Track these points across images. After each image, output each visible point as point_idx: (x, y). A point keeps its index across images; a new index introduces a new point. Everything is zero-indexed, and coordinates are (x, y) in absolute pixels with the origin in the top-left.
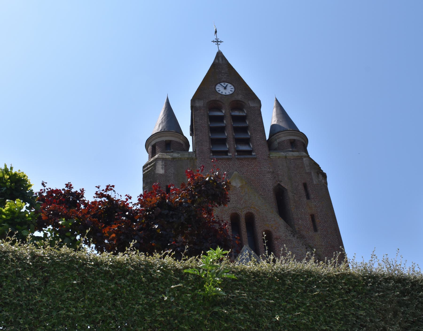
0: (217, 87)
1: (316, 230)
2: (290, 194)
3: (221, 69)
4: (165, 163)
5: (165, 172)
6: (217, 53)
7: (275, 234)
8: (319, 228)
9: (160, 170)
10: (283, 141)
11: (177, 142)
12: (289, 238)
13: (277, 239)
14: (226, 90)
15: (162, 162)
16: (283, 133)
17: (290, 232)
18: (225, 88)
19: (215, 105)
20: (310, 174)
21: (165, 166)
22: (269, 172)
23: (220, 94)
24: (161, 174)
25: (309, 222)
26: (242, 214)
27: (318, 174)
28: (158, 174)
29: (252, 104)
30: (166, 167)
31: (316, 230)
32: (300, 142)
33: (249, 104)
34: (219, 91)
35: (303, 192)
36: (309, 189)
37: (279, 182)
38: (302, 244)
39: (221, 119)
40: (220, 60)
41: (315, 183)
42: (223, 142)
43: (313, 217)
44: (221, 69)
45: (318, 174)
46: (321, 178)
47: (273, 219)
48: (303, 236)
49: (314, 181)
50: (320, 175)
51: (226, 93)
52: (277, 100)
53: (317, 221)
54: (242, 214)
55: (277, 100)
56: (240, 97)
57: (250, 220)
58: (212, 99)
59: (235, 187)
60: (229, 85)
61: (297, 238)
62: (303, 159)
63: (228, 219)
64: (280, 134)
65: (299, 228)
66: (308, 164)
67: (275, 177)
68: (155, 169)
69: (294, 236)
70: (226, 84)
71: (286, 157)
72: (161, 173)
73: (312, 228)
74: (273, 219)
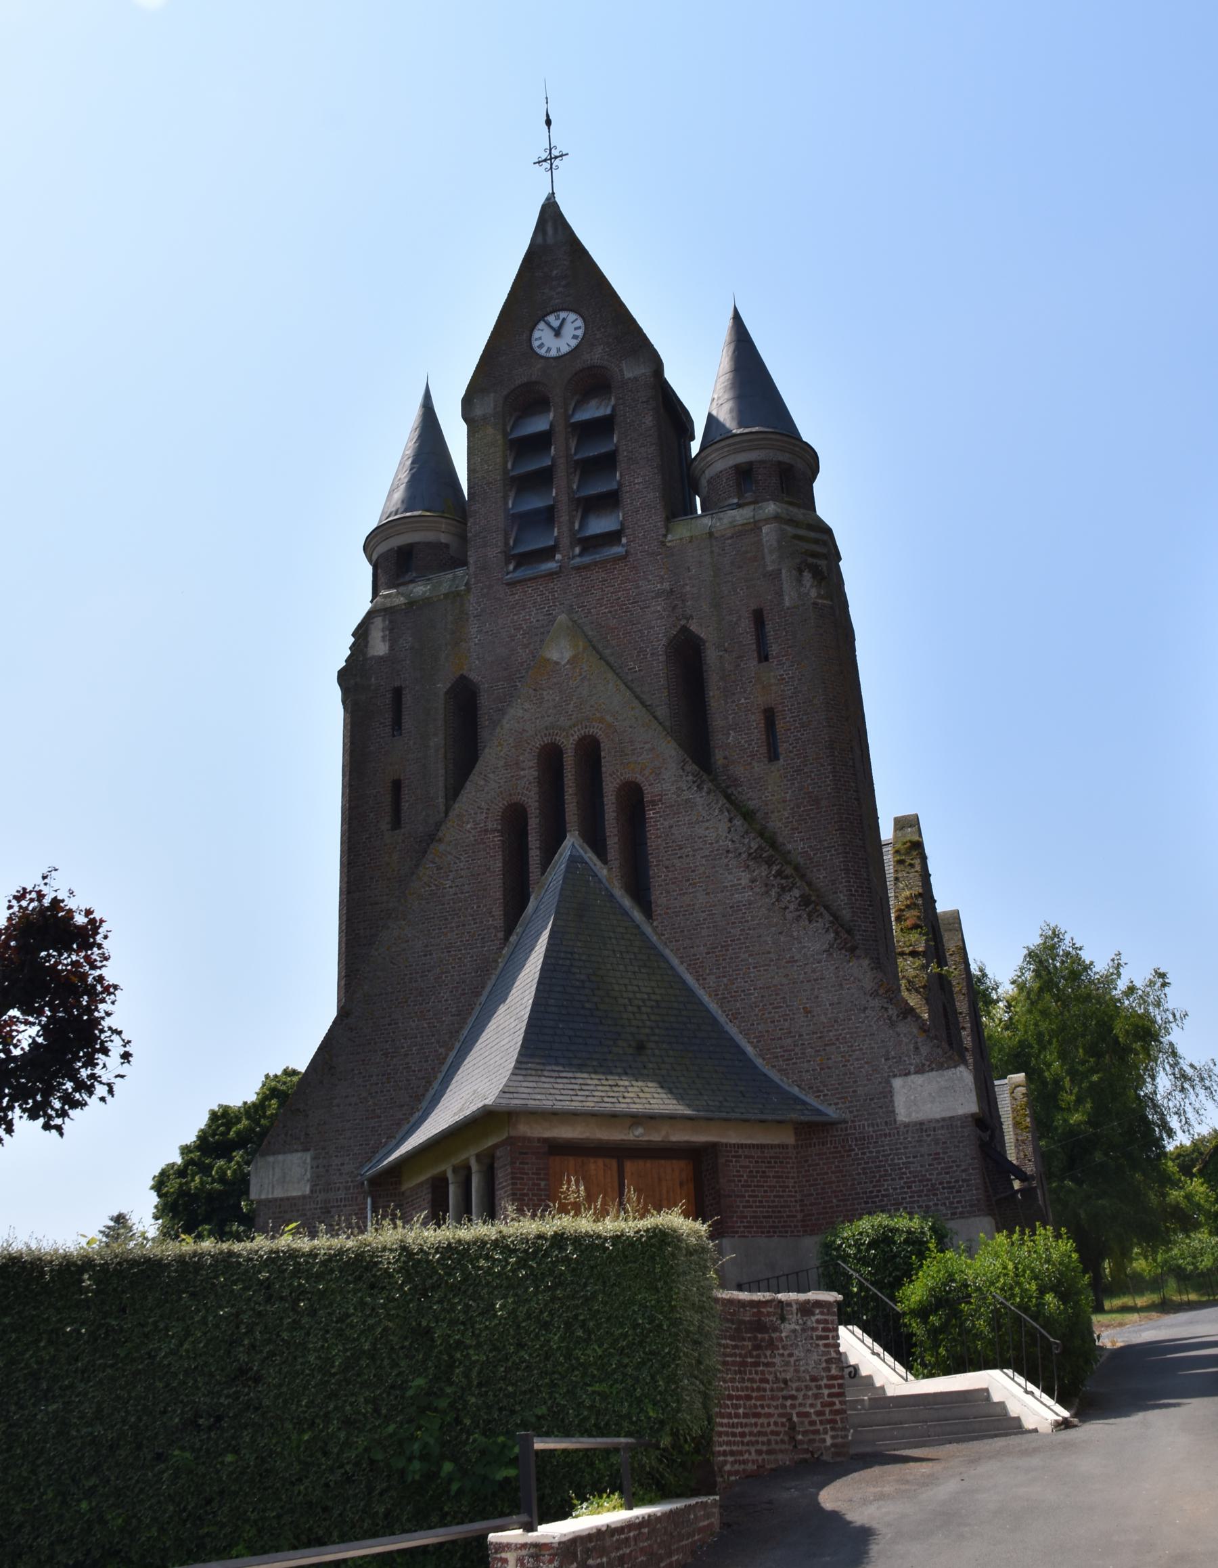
0: (536, 334)
1: (773, 756)
2: (712, 656)
3: (557, 266)
4: (391, 622)
5: (391, 648)
6: (543, 206)
7: (649, 792)
8: (782, 748)
9: (379, 647)
10: (719, 475)
11: (428, 545)
12: (687, 795)
13: (654, 803)
15: (384, 621)
16: (717, 450)
17: (690, 778)
18: (557, 333)
19: (529, 400)
20: (775, 576)
21: (391, 630)
22: (658, 595)
23: (542, 357)
24: (381, 658)
25: (757, 733)
26: (568, 743)
27: (800, 571)
28: (374, 657)
29: (631, 371)
30: (393, 635)
31: (773, 756)
32: (794, 467)
33: (621, 371)
34: (549, 350)
35: (749, 640)
36: (769, 627)
37: (683, 622)
38: (721, 810)
39: (541, 441)
40: (550, 231)
41: (787, 604)
42: (548, 516)
43: (770, 716)
44: (557, 266)
45: (800, 571)
46: (808, 585)
47: (647, 746)
48: (736, 780)
49: (787, 598)
50: (805, 574)
51: (558, 350)
52: (737, 317)
53: (780, 725)
54: (568, 743)
55: (737, 317)
56: (597, 356)
57: (590, 751)
58: (518, 382)
59: (557, 663)
60: (572, 316)
61: (708, 793)
62: (760, 529)
63: (531, 764)
64: (709, 455)
65: (725, 758)
66: (775, 544)
67: (674, 608)
68: (366, 646)
69: (700, 788)
70: (563, 315)
71: (711, 534)
72: (381, 653)
73: (764, 750)
74: (647, 746)
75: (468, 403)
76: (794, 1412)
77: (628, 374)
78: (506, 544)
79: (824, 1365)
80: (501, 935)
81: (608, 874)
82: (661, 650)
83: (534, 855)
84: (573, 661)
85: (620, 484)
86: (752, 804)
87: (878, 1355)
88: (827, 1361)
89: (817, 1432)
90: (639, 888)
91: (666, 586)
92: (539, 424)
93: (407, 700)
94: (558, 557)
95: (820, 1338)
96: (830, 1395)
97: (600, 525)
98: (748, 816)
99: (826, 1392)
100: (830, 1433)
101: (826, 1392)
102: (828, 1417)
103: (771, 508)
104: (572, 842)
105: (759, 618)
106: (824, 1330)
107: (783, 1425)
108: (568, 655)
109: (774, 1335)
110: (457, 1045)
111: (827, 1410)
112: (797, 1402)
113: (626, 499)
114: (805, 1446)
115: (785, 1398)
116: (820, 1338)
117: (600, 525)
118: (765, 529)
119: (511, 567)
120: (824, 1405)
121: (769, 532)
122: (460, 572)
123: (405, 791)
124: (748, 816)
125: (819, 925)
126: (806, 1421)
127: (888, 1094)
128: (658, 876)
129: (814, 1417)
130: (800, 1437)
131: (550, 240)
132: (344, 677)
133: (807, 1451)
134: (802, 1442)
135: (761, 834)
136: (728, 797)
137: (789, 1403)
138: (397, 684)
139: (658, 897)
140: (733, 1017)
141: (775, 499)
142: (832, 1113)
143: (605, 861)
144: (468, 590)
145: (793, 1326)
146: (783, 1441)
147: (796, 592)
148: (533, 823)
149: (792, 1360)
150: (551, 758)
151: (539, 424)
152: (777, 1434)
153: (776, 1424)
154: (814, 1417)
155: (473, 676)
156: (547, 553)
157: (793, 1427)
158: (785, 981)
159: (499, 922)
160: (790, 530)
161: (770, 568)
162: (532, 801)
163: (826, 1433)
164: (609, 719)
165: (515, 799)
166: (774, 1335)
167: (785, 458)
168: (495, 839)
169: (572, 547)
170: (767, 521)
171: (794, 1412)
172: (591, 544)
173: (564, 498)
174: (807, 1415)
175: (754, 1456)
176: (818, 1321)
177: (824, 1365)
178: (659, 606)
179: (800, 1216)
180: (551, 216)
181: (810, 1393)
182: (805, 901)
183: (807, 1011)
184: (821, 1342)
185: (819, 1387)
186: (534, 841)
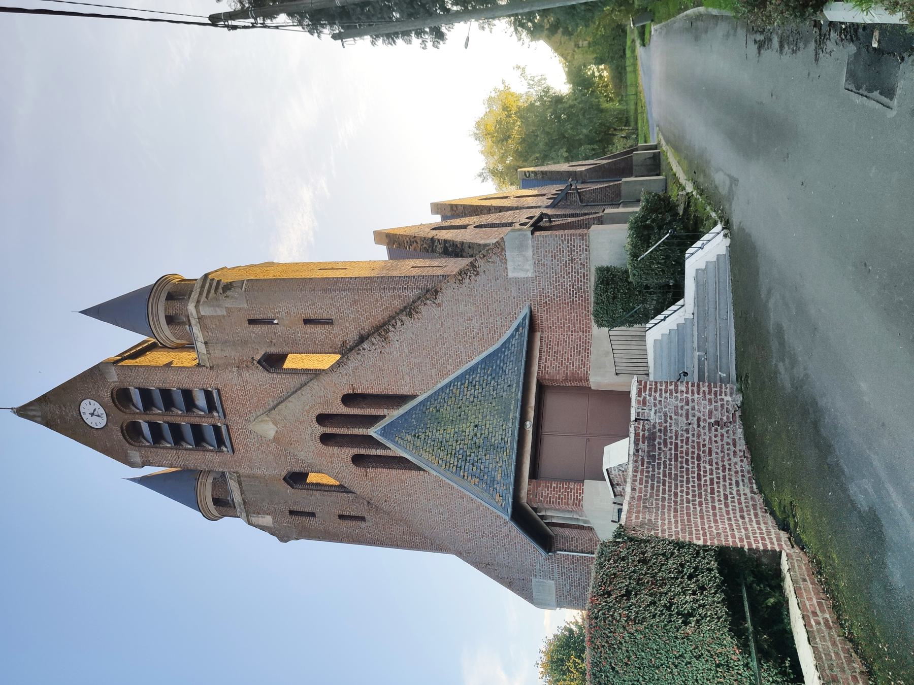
5: (268, 514)
9: (268, 520)
11: (213, 490)
14: (93, 412)
19: (132, 432)
20: (229, 310)
32: (173, 292)
37: (255, 362)
39: (155, 428)
52: (85, 312)
55: (85, 312)
56: (106, 395)
57: (322, 419)
73: (327, 327)
75: (132, 465)
76: (708, 420)
77: (116, 379)
78: (212, 451)
79: (679, 395)
80: (422, 473)
81: (393, 414)
82: (270, 376)
83: (379, 452)
84: (275, 423)
85: (178, 388)
86: (356, 338)
87: (665, 318)
88: (677, 392)
89: (722, 405)
90: (398, 400)
91: (235, 369)
92: (145, 428)
93: (295, 508)
94: (219, 424)
95: (661, 395)
96: (698, 393)
97: (201, 401)
98: (362, 339)
99: (696, 395)
100: (723, 396)
101: (696, 395)
102: (713, 396)
103: (191, 307)
104: (373, 432)
105: (252, 322)
106: (656, 391)
107: (716, 430)
108: (271, 426)
109: (658, 427)
110: (479, 500)
111: (708, 396)
112: (702, 418)
113: (186, 386)
114: (731, 415)
115: (699, 426)
116: (661, 395)
117: (201, 401)
118: (203, 313)
119: (225, 449)
120: (704, 399)
121: (205, 311)
122: (228, 475)
123: (345, 513)
124: (362, 339)
125: (422, 308)
126: (715, 412)
127: (517, 281)
128: (393, 390)
129: (712, 407)
130: (725, 418)
131: (39, 414)
132: (284, 538)
133: (734, 415)
134: (728, 417)
135: (374, 333)
136: (351, 349)
137: (702, 423)
138: (288, 513)
139: (405, 391)
140: (470, 358)
141: (186, 306)
142: (525, 311)
143: (384, 416)
144: (237, 473)
145: (652, 413)
146: (727, 432)
147: (237, 303)
148: (363, 451)
149: (674, 417)
150: (326, 439)
151: (145, 428)
152: (722, 435)
153: (716, 436)
154: (712, 407)
155: (284, 473)
156: (217, 429)
157: (717, 423)
158: (452, 329)
159: (414, 472)
160: (203, 299)
161: (225, 313)
162: (349, 452)
163: (723, 400)
164: (307, 407)
165: (350, 459)
166: (658, 427)
167: (164, 296)
168: (370, 471)
169: (213, 417)
170: (198, 312)
171: (708, 420)
172: (211, 406)
173: (186, 419)
174: (711, 412)
175: (738, 459)
176: (650, 395)
177: (679, 395)
178: (246, 374)
179: (581, 334)
180: (23, 412)
181: (696, 407)
182: (410, 315)
183: (469, 319)
184: (664, 395)
185: (693, 400)
186: (373, 452)
